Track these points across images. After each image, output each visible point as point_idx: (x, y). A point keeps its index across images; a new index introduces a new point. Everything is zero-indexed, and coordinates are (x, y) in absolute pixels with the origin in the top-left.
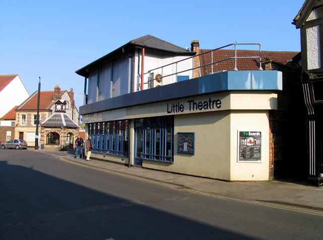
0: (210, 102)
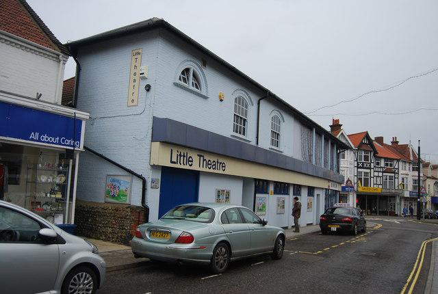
0: (218, 162)
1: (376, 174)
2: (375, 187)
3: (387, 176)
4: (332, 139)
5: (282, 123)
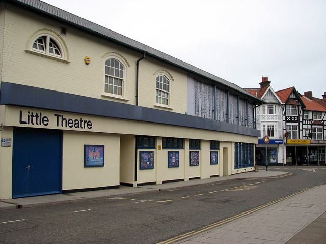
0: (81, 121)
1: (305, 127)
2: (302, 139)
3: (315, 128)
4: (250, 100)
5: (170, 82)
